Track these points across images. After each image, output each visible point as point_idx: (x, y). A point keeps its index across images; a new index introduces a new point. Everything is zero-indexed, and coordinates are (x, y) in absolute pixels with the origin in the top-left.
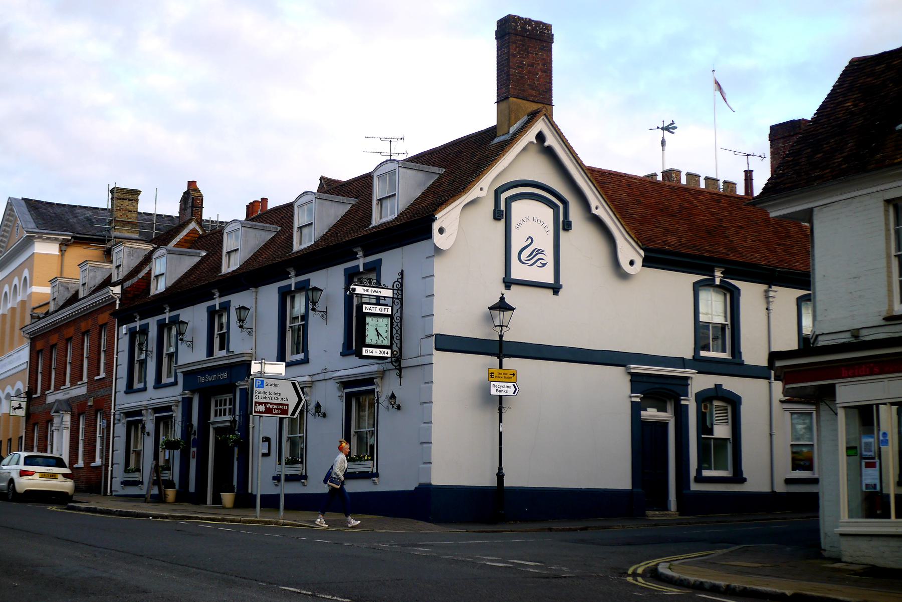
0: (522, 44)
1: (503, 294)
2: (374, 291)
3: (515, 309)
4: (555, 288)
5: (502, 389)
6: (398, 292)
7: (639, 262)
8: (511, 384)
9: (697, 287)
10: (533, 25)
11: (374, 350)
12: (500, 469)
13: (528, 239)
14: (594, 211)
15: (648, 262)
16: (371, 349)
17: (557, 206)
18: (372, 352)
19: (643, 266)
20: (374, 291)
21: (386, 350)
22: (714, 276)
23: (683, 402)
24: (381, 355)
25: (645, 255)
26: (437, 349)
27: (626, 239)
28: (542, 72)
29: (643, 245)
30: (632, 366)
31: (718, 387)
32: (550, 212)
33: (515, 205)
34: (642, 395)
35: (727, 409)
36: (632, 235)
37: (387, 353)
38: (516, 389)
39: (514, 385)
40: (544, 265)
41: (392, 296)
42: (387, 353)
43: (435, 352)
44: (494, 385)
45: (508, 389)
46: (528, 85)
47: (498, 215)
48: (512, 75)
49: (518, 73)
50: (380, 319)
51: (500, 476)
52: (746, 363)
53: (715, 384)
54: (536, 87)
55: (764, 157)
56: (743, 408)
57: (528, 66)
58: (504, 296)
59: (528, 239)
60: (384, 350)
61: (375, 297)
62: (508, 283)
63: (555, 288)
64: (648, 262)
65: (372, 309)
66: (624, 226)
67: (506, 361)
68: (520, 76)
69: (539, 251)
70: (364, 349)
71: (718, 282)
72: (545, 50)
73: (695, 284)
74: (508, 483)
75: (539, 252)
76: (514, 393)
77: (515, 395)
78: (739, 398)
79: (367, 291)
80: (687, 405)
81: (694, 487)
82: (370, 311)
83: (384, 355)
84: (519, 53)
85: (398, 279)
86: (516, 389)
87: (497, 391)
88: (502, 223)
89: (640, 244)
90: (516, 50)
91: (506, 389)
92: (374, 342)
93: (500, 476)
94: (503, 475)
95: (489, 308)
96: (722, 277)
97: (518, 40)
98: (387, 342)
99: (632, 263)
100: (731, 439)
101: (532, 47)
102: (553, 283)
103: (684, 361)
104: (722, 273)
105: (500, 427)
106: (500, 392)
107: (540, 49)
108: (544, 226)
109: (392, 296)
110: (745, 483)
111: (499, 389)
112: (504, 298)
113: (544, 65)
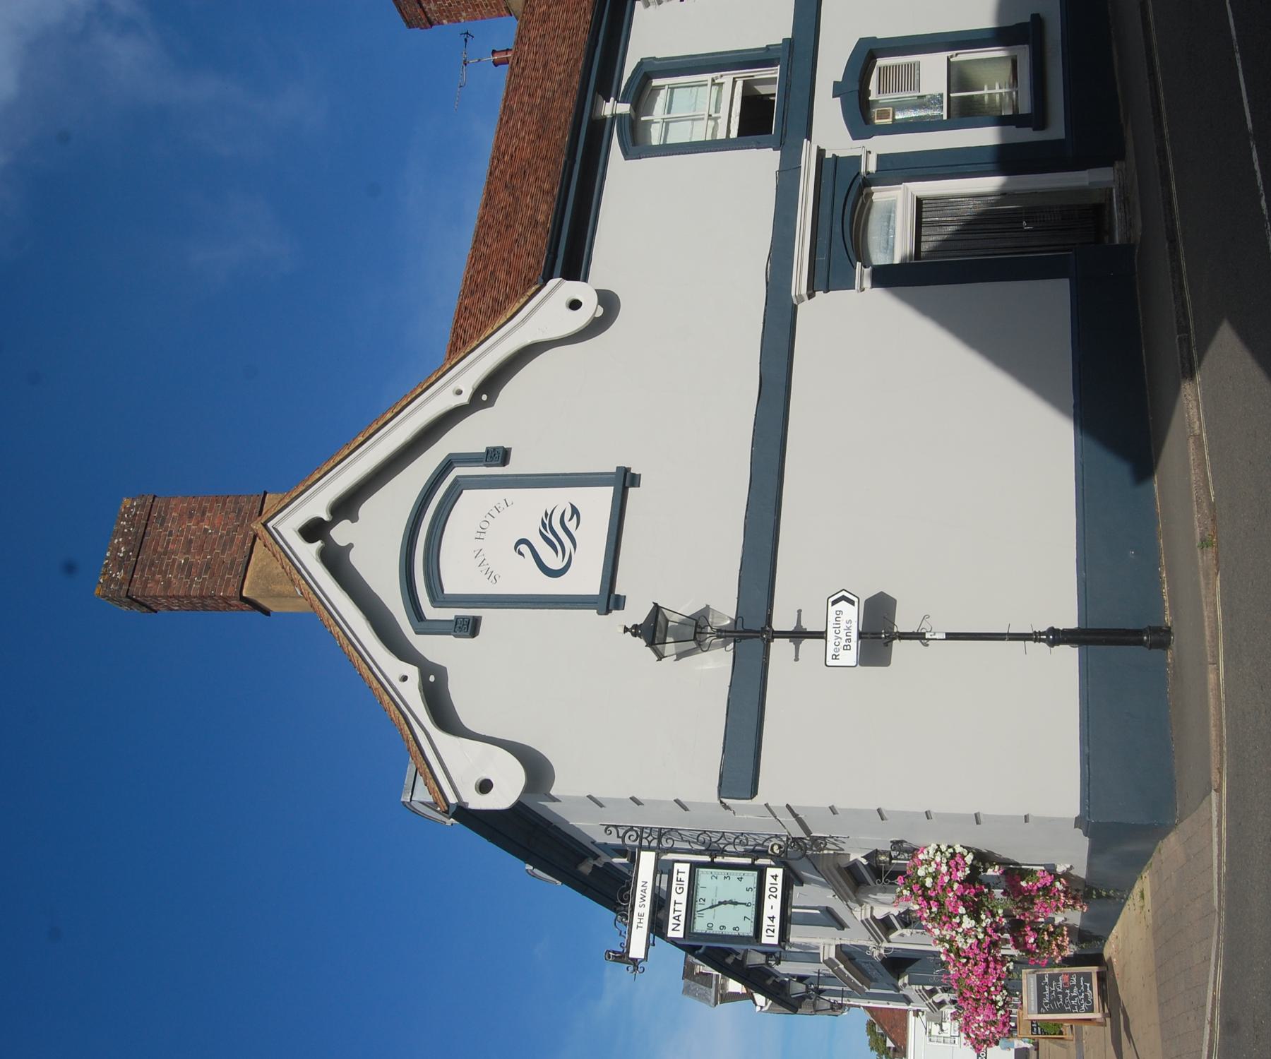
0: (150, 569)
1: (626, 630)
2: (643, 899)
3: (656, 605)
4: (625, 481)
5: (842, 634)
6: (646, 838)
7: (573, 289)
8: (832, 609)
9: (637, 146)
10: (119, 541)
11: (767, 912)
12: (1034, 637)
13: (520, 553)
14: (464, 399)
15: (575, 268)
16: (766, 922)
17: (456, 481)
18: (772, 918)
19: (585, 280)
20: (643, 899)
21: (769, 880)
22: (614, 116)
23: (872, 168)
24: (779, 893)
25: (560, 277)
26: (754, 793)
27: (524, 321)
28: (203, 521)
29: (536, 284)
30: (793, 294)
31: (838, 90)
32: (469, 498)
33: (452, 584)
34: (859, 264)
35: (886, 68)
36: (515, 310)
37: (775, 876)
38: (844, 598)
39: (834, 603)
40: (575, 511)
41: (653, 854)
42: (775, 877)
43: (759, 800)
44: (835, 657)
45: (843, 618)
46: (223, 552)
47: (470, 628)
48: (202, 589)
49: (199, 577)
50: (701, 894)
51: (1056, 637)
52: (788, 34)
53: (834, 97)
54: (228, 534)
55: (467, 33)
56: (881, 34)
57: (188, 552)
58: (629, 627)
59: (520, 553)
60: (768, 886)
61: (658, 875)
62: (609, 601)
63: (625, 481)
64: (575, 268)
65: (677, 914)
66: (495, 328)
67: (777, 625)
68: (206, 573)
69: (546, 524)
70: (765, 940)
71: (624, 108)
72: (166, 512)
73: (627, 155)
74: (1070, 621)
75: (547, 523)
76: (852, 603)
77: (855, 599)
78: (862, 42)
79: (641, 916)
80: (880, 158)
81: (1056, 130)
82: (682, 919)
83: (779, 887)
84: (164, 573)
85: (618, 837)
86: (844, 598)
87: (847, 648)
88: (489, 617)
89: (534, 289)
90: (158, 582)
91: (843, 625)
92: (750, 912)
93: (1056, 637)
94: (1052, 631)
95: (660, 659)
96: (616, 99)
97: (142, 576)
98: (751, 878)
99: (575, 305)
100: (949, 53)
101: (157, 544)
102: (613, 488)
103: (782, 171)
104: (608, 101)
105: (936, 639)
106: (849, 640)
107: (161, 525)
108: (494, 513)
109: (653, 854)
110: (1041, 15)
111: (843, 643)
112: (635, 627)
113: (191, 516)
